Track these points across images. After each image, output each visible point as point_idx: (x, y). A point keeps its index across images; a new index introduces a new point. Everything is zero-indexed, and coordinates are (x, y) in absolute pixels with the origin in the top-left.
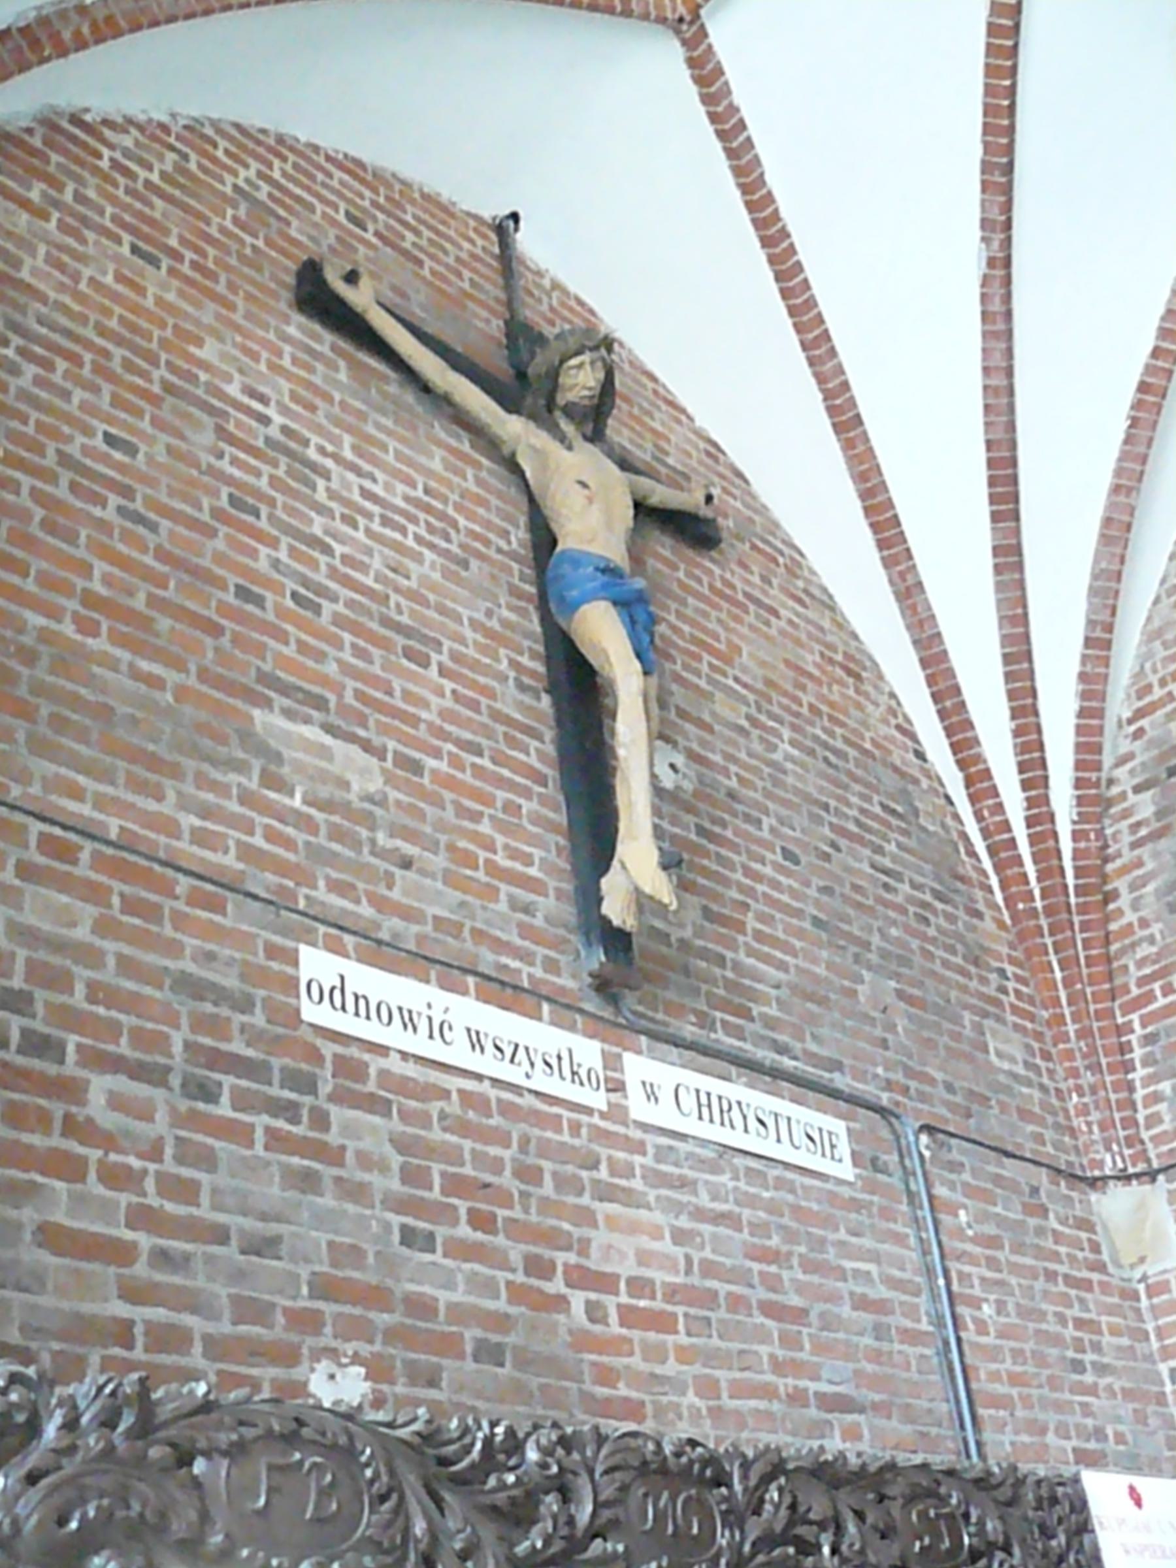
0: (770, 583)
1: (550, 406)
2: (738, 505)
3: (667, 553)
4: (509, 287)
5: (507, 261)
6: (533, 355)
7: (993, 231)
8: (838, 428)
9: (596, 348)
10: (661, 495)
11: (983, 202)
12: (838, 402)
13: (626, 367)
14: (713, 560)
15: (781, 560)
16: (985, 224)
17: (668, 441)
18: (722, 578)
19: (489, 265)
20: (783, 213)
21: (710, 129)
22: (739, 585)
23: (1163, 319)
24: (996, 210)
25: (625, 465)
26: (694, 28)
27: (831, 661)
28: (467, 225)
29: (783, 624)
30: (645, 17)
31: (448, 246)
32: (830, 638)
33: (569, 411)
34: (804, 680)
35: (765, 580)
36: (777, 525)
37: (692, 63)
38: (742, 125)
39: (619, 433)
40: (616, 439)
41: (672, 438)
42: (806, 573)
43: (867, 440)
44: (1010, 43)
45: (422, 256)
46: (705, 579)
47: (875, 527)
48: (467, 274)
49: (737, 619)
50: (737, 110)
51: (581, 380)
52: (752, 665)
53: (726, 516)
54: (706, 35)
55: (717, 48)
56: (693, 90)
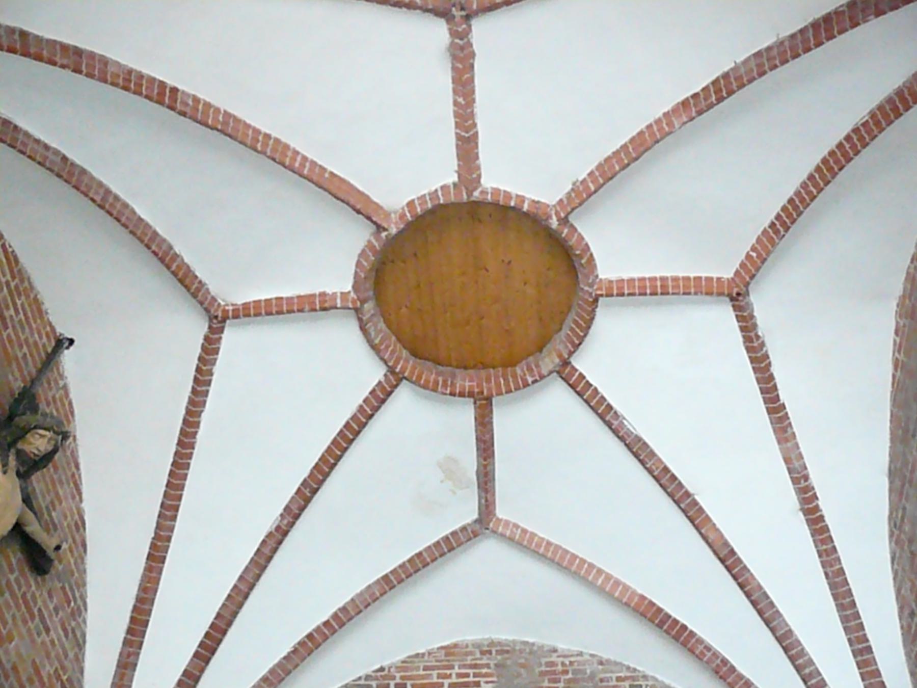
0: (57, 614)
1: (13, 444)
2: (72, 561)
3: (14, 561)
4: (40, 371)
5: (51, 358)
6: (24, 414)
7: (289, 514)
8: (150, 557)
9: (57, 433)
10: (34, 528)
11: (293, 498)
12: (159, 544)
13: (68, 453)
14: (36, 580)
15: (72, 604)
16: (287, 509)
17: (61, 503)
18: (33, 596)
19: (39, 354)
20: (198, 436)
21: (193, 373)
22: (40, 603)
23: (340, 609)
24: (296, 506)
25: (27, 500)
26: (219, 325)
27: (59, 678)
28: (45, 328)
29: (47, 640)
30: (201, 303)
31: (27, 330)
32: (67, 664)
33: (20, 454)
34: (35, 679)
35: (56, 609)
36: (84, 585)
37: (206, 338)
38: (209, 383)
39: (38, 482)
40: (35, 484)
41: (64, 504)
42: (80, 620)
43: (160, 573)
44: (345, 445)
45: (10, 325)
46: (24, 589)
47: (133, 620)
48: (25, 349)
49: (25, 622)
50: (212, 375)
51: (38, 443)
52: (13, 653)
53: (60, 562)
54: (222, 332)
55: (223, 341)
56: (198, 351)
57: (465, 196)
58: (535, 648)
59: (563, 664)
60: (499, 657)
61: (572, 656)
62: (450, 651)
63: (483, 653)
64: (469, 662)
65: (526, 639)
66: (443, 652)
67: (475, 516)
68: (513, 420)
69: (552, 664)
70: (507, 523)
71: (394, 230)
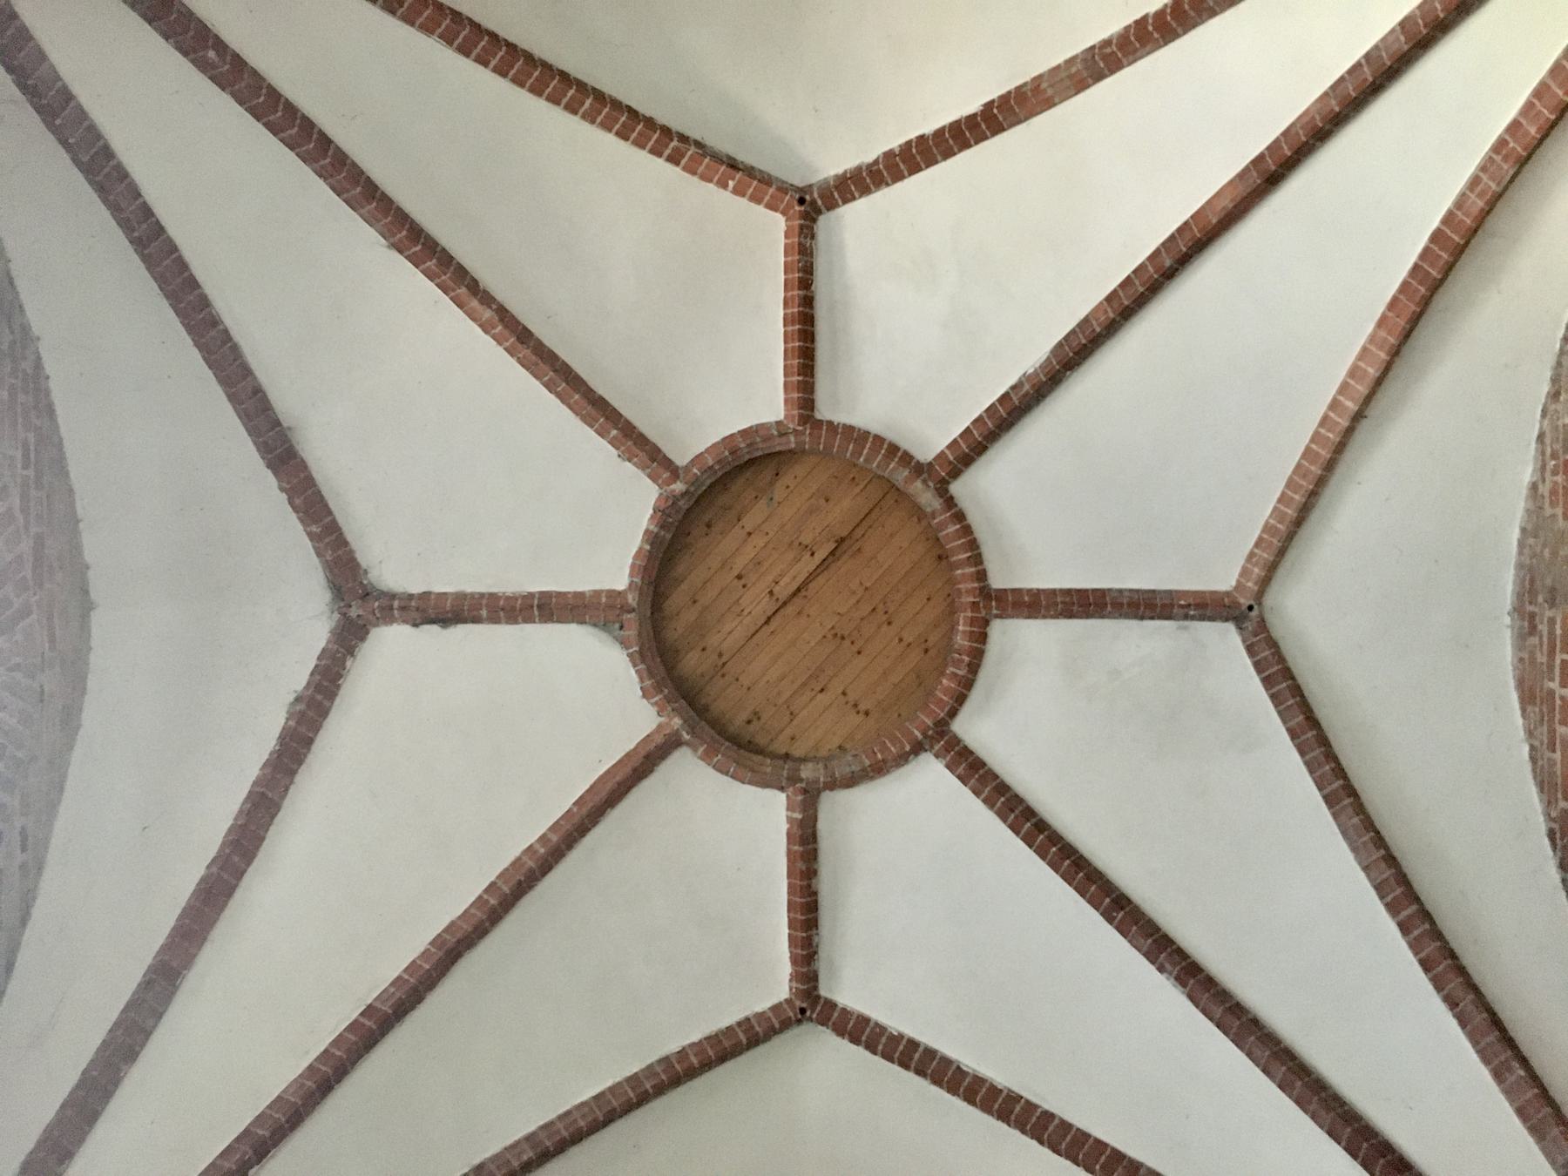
57: (632, 615)
58: (1529, 527)
59: (1555, 472)
60: (1540, 599)
61: (1543, 453)
62: (1528, 696)
63: (1533, 629)
64: (1545, 660)
65: (1515, 543)
66: (1529, 708)
67: (1230, 627)
68: (1029, 552)
69: (1553, 492)
70: (1245, 572)
71: (677, 722)
